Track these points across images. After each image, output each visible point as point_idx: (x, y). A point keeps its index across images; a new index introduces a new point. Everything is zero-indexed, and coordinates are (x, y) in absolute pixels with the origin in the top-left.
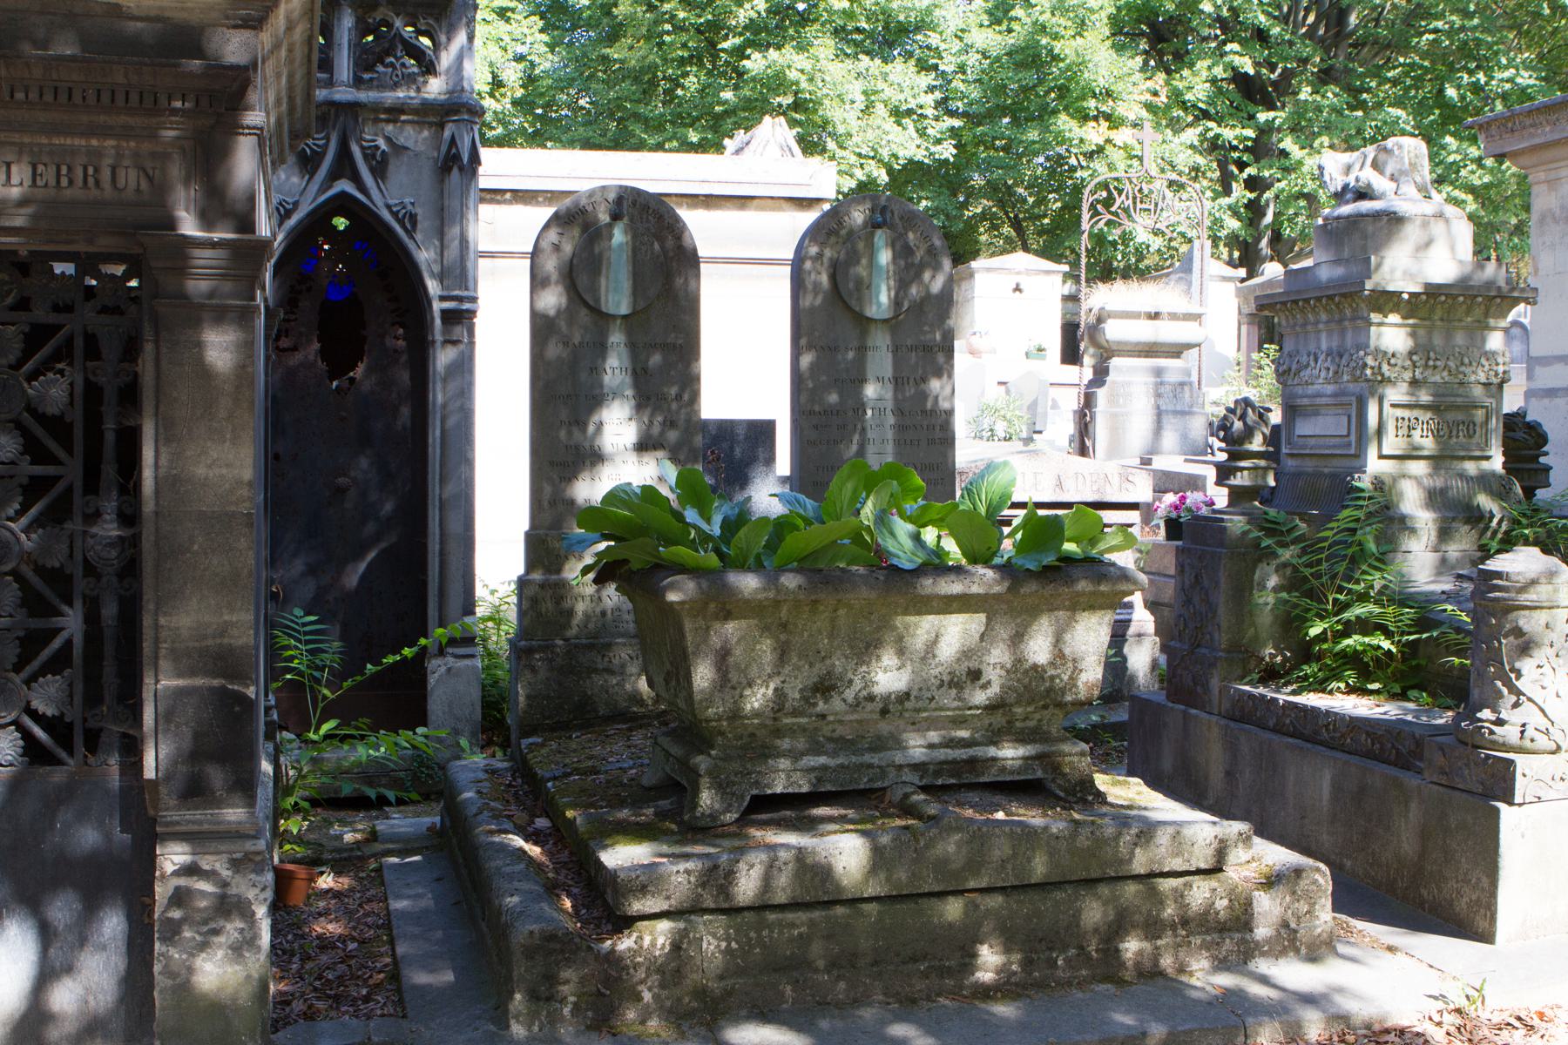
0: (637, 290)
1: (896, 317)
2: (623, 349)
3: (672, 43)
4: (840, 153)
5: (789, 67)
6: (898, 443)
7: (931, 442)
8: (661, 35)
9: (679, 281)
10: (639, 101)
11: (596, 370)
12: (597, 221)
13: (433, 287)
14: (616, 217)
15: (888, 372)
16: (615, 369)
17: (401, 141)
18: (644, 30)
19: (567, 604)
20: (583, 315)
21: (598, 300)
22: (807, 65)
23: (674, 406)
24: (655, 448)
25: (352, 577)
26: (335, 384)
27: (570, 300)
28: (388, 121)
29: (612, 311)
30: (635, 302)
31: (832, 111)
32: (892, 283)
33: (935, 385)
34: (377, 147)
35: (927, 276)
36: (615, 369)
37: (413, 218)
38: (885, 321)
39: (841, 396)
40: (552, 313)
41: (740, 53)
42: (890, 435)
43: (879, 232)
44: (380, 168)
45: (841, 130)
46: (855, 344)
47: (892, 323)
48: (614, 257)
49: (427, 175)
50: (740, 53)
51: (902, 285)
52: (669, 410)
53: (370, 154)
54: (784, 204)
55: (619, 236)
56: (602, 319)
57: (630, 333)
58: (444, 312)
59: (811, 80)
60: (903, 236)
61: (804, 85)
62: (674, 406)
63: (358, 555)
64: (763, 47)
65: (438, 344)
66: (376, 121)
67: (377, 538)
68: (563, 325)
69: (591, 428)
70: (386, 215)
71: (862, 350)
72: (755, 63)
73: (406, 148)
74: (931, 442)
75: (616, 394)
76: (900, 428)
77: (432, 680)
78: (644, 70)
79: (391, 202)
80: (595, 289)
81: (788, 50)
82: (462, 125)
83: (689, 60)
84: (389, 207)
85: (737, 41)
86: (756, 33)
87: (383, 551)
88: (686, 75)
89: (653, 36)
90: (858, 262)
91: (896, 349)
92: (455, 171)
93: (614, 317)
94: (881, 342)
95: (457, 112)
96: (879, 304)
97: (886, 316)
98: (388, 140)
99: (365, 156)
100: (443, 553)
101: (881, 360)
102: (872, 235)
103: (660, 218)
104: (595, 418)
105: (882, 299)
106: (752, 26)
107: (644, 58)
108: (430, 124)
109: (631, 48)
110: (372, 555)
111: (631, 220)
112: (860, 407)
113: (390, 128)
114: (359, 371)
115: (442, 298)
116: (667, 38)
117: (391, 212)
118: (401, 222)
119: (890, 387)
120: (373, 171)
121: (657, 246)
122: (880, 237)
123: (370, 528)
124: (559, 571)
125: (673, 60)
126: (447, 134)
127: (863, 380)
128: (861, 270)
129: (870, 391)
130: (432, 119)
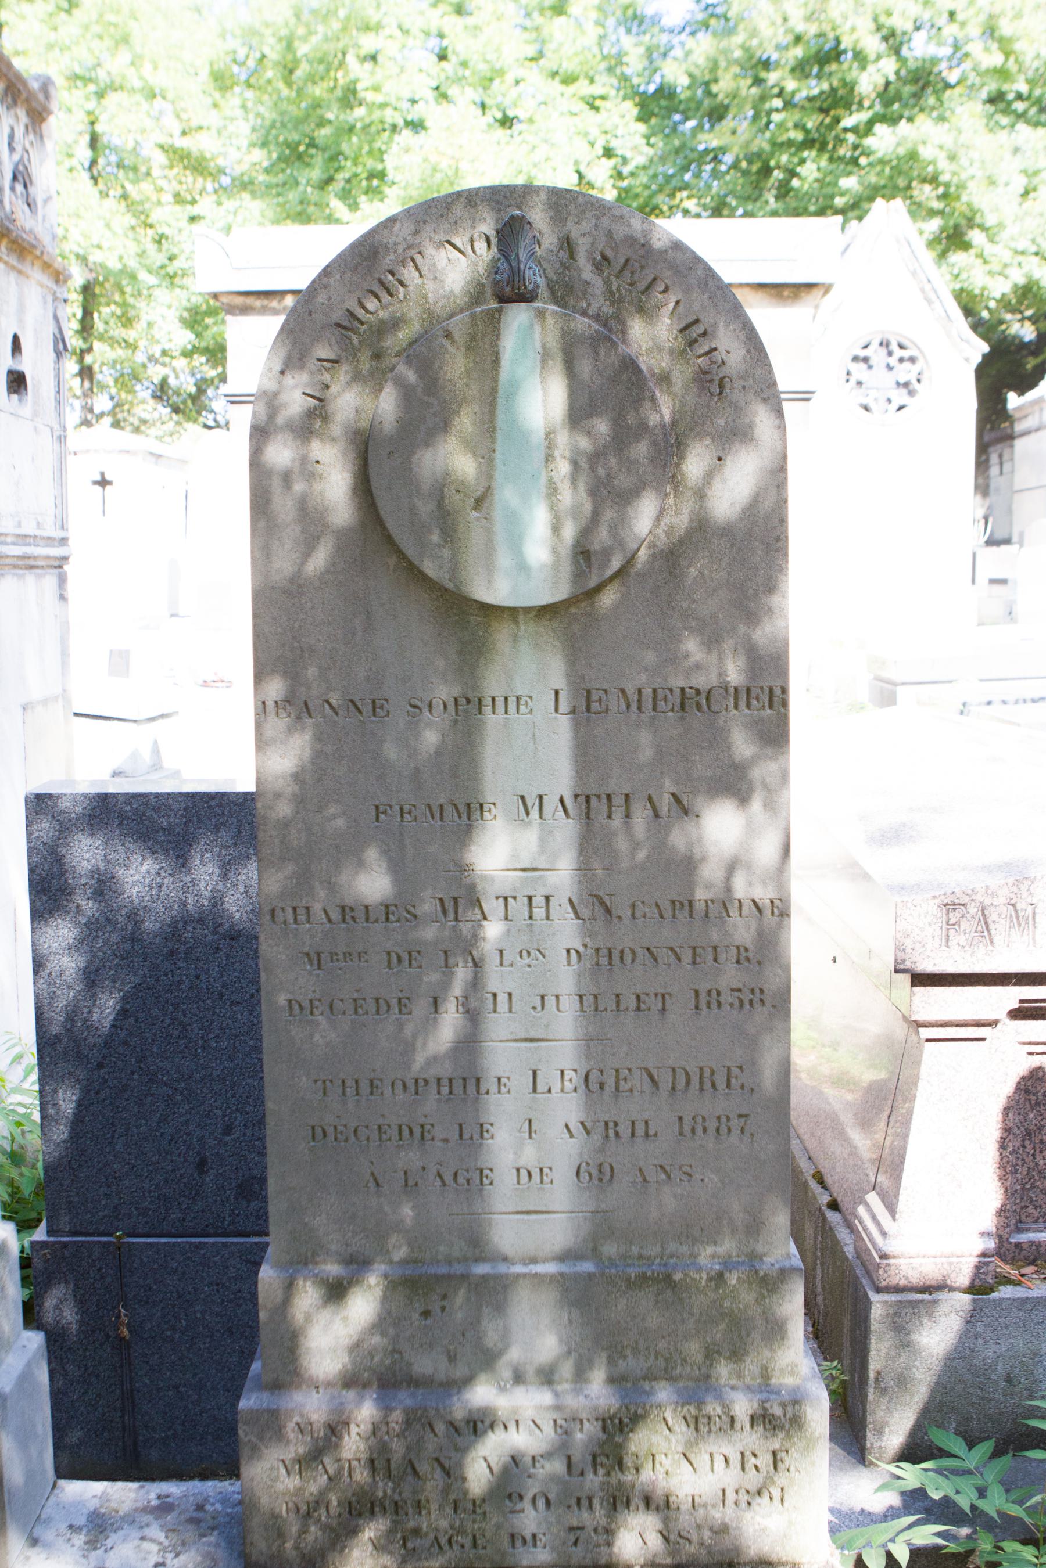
1: (586, 595)
4: (989, 249)
5: (924, 143)
6: (591, 1004)
7: (706, 1000)
8: (769, 113)
15: (559, 778)
22: (948, 140)
31: (976, 196)
32: (566, 496)
33: (720, 828)
35: (695, 465)
38: (545, 612)
39: (396, 868)
42: (566, 980)
43: (518, 318)
45: (990, 221)
46: (444, 692)
47: (564, 617)
51: (607, 487)
60: (610, 329)
61: (943, 164)
64: (893, 120)
71: (469, 708)
72: (884, 141)
74: (706, 1000)
76: (603, 961)
81: (921, 119)
85: (863, 116)
88: (803, 161)
90: (444, 426)
91: (586, 706)
94: (530, 679)
96: (522, 567)
97: (545, 597)
101: (532, 734)
102: (493, 321)
105: (525, 551)
107: (748, 143)
112: (463, 898)
116: (776, 117)
119: (565, 831)
122: (524, 333)
127: (466, 814)
128: (455, 459)
129: (497, 853)
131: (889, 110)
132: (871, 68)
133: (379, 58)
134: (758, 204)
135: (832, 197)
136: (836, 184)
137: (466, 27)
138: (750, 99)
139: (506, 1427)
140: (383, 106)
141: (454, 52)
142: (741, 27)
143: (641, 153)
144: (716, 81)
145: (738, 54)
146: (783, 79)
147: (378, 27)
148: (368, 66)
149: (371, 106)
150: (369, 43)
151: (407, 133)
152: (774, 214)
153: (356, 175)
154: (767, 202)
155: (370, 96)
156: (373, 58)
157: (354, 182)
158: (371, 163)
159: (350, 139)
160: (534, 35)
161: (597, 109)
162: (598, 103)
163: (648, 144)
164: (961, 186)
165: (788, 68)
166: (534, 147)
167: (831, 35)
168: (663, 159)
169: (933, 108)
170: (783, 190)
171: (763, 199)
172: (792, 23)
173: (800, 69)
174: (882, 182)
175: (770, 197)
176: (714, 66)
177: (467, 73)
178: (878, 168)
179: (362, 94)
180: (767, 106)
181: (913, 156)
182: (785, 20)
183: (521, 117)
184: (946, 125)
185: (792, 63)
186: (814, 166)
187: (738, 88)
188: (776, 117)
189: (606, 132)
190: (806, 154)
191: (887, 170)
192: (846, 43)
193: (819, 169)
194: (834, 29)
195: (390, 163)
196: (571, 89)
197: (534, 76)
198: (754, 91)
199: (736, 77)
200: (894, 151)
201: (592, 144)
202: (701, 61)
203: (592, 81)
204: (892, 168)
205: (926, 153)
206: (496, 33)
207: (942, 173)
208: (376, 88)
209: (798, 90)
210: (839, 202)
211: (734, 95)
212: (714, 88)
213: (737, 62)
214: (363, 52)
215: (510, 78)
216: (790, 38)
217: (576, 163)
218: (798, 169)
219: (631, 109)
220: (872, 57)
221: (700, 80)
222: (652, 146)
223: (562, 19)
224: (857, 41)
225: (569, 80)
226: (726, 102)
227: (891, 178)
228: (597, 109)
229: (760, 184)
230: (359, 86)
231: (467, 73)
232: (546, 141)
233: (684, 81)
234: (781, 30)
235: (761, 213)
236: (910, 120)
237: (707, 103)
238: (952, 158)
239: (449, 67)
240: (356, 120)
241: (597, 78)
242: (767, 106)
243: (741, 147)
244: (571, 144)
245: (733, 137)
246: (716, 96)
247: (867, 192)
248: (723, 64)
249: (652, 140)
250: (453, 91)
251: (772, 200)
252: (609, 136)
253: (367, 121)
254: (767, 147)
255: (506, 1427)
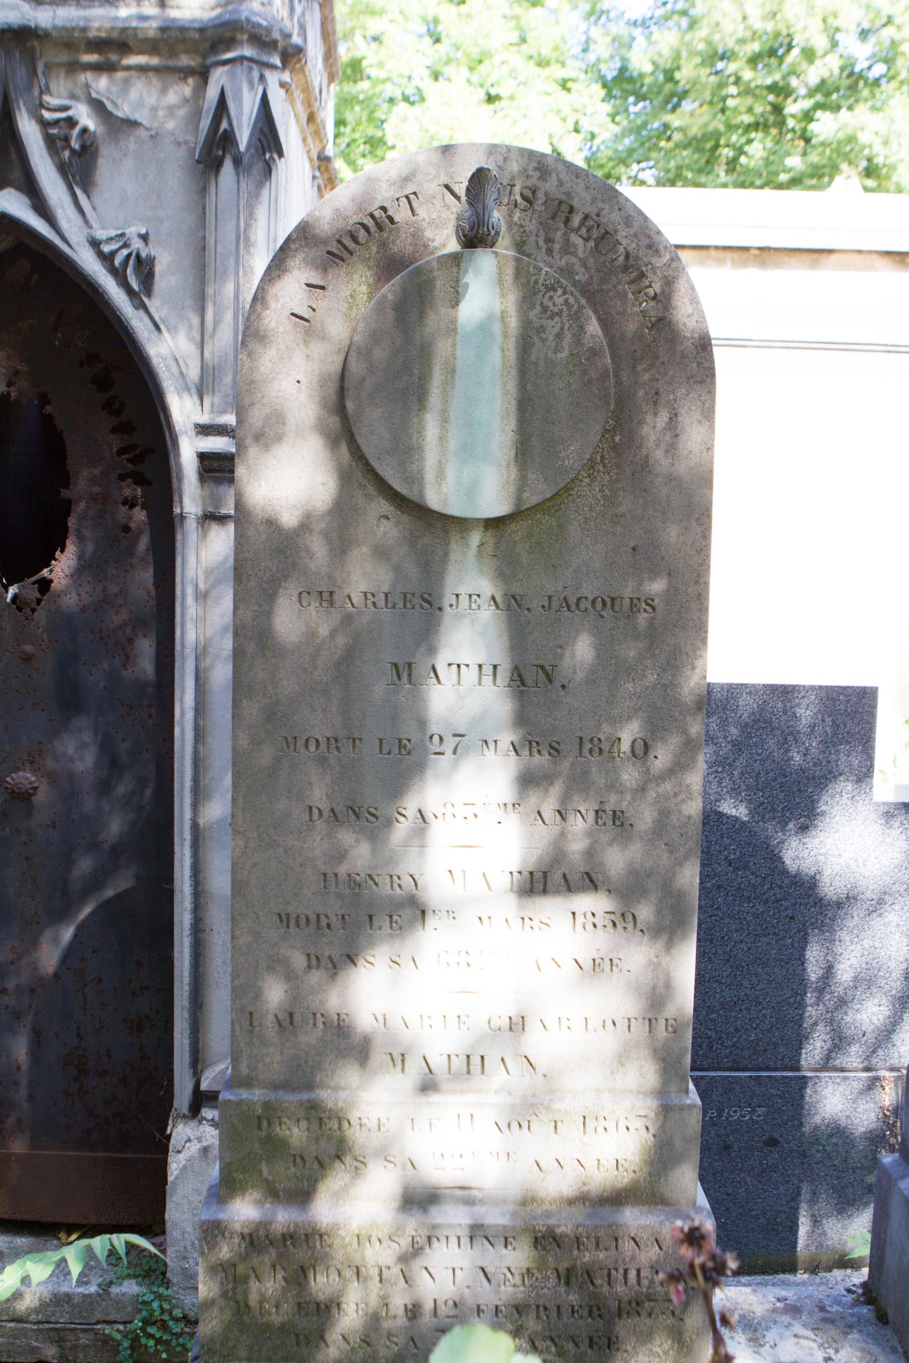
0: (532, 441)
2: (487, 614)
3: (735, 109)
8: (724, 99)
9: (652, 427)
10: (700, 171)
11: (408, 672)
12: (420, 244)
13: (183, 411)
14: (475, 237)
16: (465, 672)
17: (124, 110)
18: (707, 95)
19: (321, 1284)
20: (381, 525)
21: (417, 480)
23: (629, 776)
24: (569, 887)
25: (49, 956)
26: (12, 590)
27: (345, 479)
28: (97, 68)
29: (455, 509)
30: (522, 484)
34: (71, 122)
36: (465, 672)
37: (145, 268)
40: (289, 519)
41: (808, 117)
44: (79, 163)
48: (464, 355)
49: (174, 177)
50: (808, 117)
52: (614, 786)
53: (57, 136)
54: (878, 261)
55: (484, 297)
56: (432, 528)
57: (506, 568)
58: (203, 457)
59: (886, 143)
61: (878, 149)
62: (629, 776)
63: (59, 916)
65: (191, 524)
66: (74, 67)
67: (95, 883)
68: (318, 550)
69: (401, 829)
70: (89, 262)
72: (825, 126)
73: (133, 124)
75: (462, 742)
77: (175, 1165)
78: (706, 137)
79: (101, 234)
80: (407, 449)
81: (862, 109)
82: (239, 69)
83: (755, 126)
84: (95, 244)
85: (807, 104)
86: (828, 94)
87: (107, 905)
88: (750, 141)
89: (718, 103)
92: (228, 166)
93: (463, 524)
94: (472, 589)
95: (230, 43)
98: (98, 106)
99: (51, 143)
100: (198, 928)
103: (604, 238)
104: (410, 805)
106: (823, 88)
107: (707, 124)
108: (185, 73)
109: (692, 115)
110: (87, 910)
111: (520, 246)
113: (101, 84)
114: (62, 568)
115: (204, 430)
117: (101, 255)
118: (119, 275)
120: (63, 169)
121: (593, 327)
123: (85, 865)
124: (303, 1195)
125: (737, 127)
126: (212, 93)
130: (185, 61)
131: (828, 100)
132: (818, 63)
133: (385, 39)
134: (711, 177)
135: (777, 174)
136: (782, 163)
137: (459, 15)
138: (709, 86)
139: (438, 1240)
140: (384, 81)
141: (447, 36)
142: (705, 22)
143: (608, 130)
144: (678, 68)
145: (701, 46)
146: (741, 69)
147: (382, 12)
148: (374, 45)
149: (377, 82)
150: (374, 26)
151: (403, 105)
152: (725, 186)
153: (354, 141)
154: (718, 176)
155: (373, 72)
156: (375, 39)
157: (353, 146)
158: (371, 131)
159: (352, 108)
160: (513, 23)
161: (569, 90)
162: (569, 85)
163: (613, 121)
164: (892, 168)
165: (745, 59)
166: (515, 122)
167: (785, 32)
168: (624, 134)
169: (866, 100)
170: (731, 166)
171: (715, 173)
172: (751, 21)
173: (753, 61)
174: (824, 162)
175: (721, 171)
176: (677, 56)
177: (459, 54)
178: (820, 149)
179: (368, 71)
180: (724, 92)
181: (851, 139)
182: (745, 18)
183: (502, 95)
184: (881, 114)
185: (749, 54)
186: (761, 146)
187: (699, 76)
188: (730, 103)
189: (576, 111)
190: (753, 135)
191: (828, 152)
192: (798, 40)
193: (764, 148)
194: (788, 27)
195: (390, 132)
196: (546, 72)
197: (516, 59)
198: (713, 79)
199: (696, 67)
200: (835, 135)
201: (564, 120)
202: (666, 52)
203: (563, 64)
204: (832, 150)
205: (864, 138)
206: (487, 22)
207: (877, 155)
208: (381, 65)
209: (754, 79)
210: (783, 177)
211: (695, 82)
212: (677, 76)
213: (699, 53)
214: (370, 33)
215: (497, 60)
216: (748, 34)
217: (551, 136)
218: (746, 148)
219: (598, 91)
220: (820, 52)
221: (662, 67)
222: (618, 124)
223: (538, 9)
224: (807, 40)
225: (542, 63)
226: (687, 87)
227: (830, 159)
228: (569, 90)
229: (704, 160)
230: (364, 64)
231: (459, 54)
232: (525, 116)
233: (648, 68)
234: (742, 26)
235: (713, 184)
236: (850, 108)
237: (668, 87)
238: (886, 143)
239: (442, 48)
240: (359, 93)
241: (568, 62)
242: (724, 92)
243: (700, 128)
244: (566, 124)
245: (690, 117)
246: (677, 82)
247: (809, 171)
248: (684, 55)
249: (618, 119)
250: (447, 71)
251: (722, 174)
252: (579, 114)
253: (370, 93)
254: (722, 128)
255: (438, 1240)
